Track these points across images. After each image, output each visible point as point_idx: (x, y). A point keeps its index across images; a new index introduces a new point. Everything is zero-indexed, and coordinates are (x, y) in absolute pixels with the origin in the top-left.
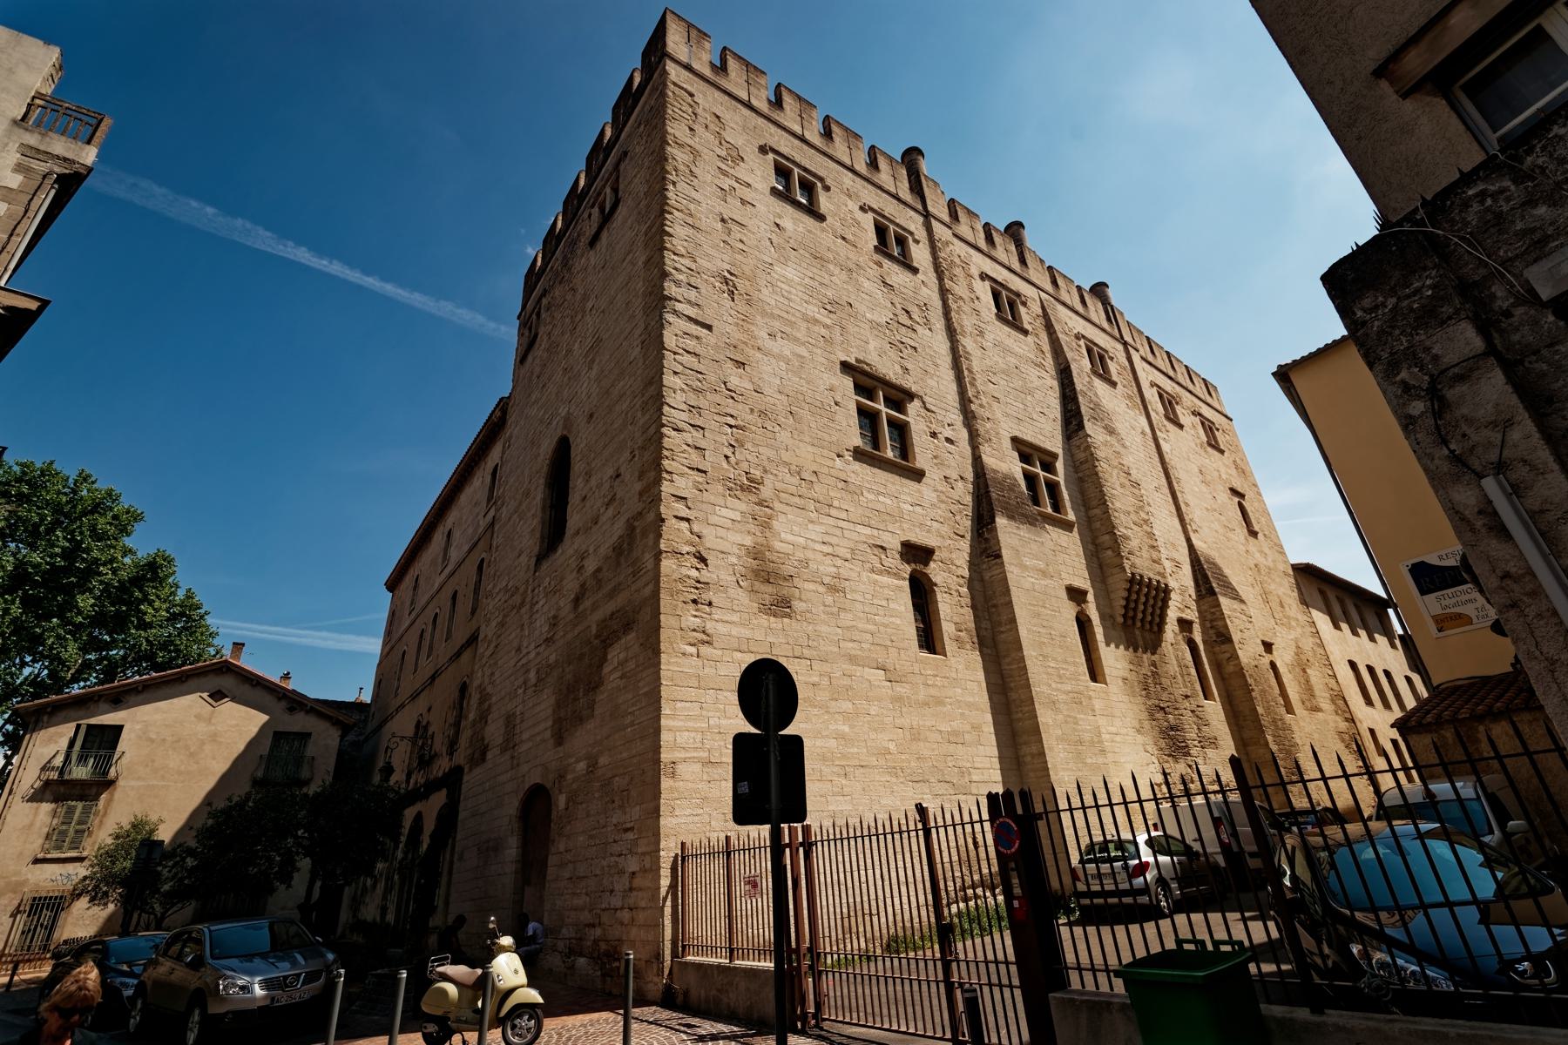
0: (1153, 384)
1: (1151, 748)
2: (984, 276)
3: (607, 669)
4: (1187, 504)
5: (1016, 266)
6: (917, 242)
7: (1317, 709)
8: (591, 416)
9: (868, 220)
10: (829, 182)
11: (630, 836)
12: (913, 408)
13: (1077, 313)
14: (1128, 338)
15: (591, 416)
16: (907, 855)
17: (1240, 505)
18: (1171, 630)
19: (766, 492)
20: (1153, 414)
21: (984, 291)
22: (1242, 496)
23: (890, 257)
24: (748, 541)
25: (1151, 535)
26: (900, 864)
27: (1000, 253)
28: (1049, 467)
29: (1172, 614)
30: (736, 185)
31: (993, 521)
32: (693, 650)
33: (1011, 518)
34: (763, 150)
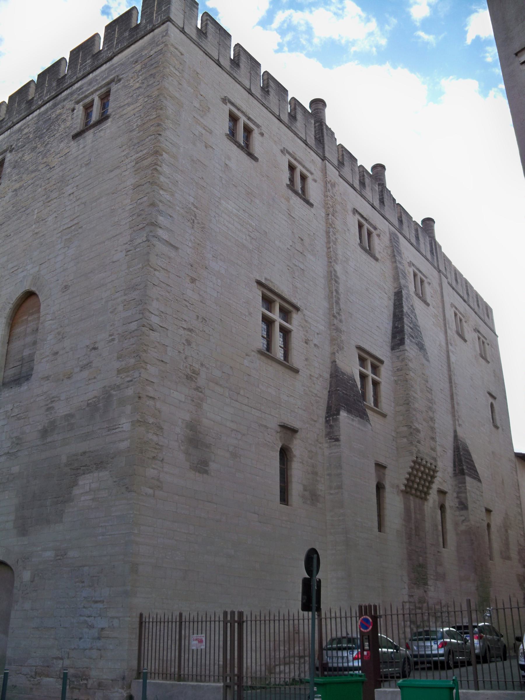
0: (452, 305)
1: (406, 579)
2: (355, 211)
3: (76, 491)
4: (458, 404)
5: (377, 204)
6: (315, 181)
7: (508, 558)
8: (66, 287)
9: (284, 161)
10: (264, 130)
11: (100, 605)
12: (296, 317)
13: (412, 244)
14: (442, 268)
15: (66, 287)
16: (258, 634)
17: (492, 405)
18: (433, 497)
19: (201, 381)
20: (449, 331)
21: (353, 221)
22: (494, 398)
23: (296, 192)
24: (187, 417)
25: (433, 429)
26: (254, 639)
27: (368, 193)
28: (375, 369)
29: (435, 487)
30: (204, 132)
31: (338, 414)
32: (150, 491)
33: (349, 412)
34: (225, 100)
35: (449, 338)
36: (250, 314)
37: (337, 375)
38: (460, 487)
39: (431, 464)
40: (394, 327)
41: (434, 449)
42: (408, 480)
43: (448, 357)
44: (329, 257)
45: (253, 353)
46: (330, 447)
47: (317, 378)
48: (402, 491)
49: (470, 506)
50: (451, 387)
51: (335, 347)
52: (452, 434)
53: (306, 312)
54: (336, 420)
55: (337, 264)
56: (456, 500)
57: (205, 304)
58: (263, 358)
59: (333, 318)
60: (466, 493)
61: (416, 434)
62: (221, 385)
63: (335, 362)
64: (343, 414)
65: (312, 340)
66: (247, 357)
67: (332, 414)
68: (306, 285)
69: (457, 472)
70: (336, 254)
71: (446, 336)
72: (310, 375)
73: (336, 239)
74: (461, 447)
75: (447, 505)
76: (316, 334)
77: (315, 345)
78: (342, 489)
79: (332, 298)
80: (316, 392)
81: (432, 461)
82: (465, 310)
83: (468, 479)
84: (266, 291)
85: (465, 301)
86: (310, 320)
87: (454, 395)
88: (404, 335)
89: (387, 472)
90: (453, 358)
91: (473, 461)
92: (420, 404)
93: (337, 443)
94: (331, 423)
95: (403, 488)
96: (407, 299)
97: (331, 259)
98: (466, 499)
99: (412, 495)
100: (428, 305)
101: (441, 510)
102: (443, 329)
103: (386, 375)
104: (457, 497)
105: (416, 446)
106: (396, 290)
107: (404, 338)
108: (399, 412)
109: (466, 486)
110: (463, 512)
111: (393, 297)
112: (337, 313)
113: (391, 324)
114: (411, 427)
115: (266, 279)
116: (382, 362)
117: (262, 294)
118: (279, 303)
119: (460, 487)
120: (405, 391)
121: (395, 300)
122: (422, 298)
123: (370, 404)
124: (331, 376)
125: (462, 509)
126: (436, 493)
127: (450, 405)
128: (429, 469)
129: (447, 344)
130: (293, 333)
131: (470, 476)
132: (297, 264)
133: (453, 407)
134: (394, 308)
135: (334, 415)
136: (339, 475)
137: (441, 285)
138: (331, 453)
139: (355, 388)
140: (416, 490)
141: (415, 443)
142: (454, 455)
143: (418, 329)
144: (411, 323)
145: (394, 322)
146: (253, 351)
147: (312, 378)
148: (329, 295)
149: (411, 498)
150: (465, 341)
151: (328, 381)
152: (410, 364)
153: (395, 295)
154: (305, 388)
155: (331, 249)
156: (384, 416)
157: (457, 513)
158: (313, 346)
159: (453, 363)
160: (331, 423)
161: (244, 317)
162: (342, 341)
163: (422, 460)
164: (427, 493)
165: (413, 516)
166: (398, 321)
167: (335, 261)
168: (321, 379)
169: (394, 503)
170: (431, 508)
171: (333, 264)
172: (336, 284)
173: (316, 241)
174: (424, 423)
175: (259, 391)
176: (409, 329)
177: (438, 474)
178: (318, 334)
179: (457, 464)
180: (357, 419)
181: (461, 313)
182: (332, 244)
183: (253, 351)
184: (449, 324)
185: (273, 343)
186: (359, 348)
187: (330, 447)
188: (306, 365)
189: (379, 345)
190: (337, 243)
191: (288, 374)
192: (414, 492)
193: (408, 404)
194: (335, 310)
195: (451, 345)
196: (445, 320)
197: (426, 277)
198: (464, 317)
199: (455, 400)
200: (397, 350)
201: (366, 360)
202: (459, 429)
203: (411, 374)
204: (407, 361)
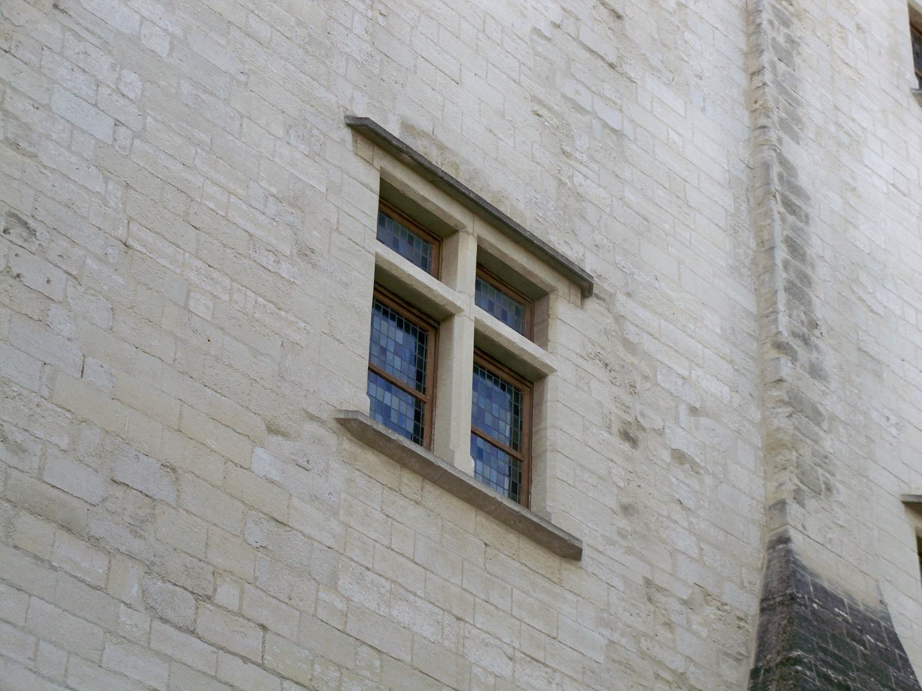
36: (305, 253)
37: (793, 598)
44: (756, 106)
45: (311, 428)
47: (684, 602)
51: (784, 476)
53: (624, 305)
55: (796, 138)
57: (33, 156)
58: (370, 458)
59: (774, 353)
62: (94, 542)
65: (660, 433)
66: (275, 439)
68: (630, 196)
70: (793, 102)
72: (648, 583)
73: (791, 40)
76: (683, 411)
77: (679, 457)
79: (770, 269)
80: (678, 664)
84: (403, 177)
86: (648, 345)
97: (768, 110)
112: (794, 335)
115: (407, 126)
117: (383, 182)
118: (480, 240)
124: (767, 606)
130: (551, 382)
132: (585, 100)
139: (892, 671)
146: (313, 418)
147: (657, 596)
148: (754, 262)
151: (752, 629)
154: (616, 637)
155: (768, 77)
158: (666, 456)
161: (269, 260)
162: (824, 459)
167: (785, 126)
168: (710, 611)
171: (773, 135)
172: (791, 218)
173: (688, 36)
175: (340, 605)
178: (694, 411)
182: (768, 57)
183: (313, 418)
185: (439, 411)
188: (622, 534)
190: (797, 60)
191: (520, 558)
194: (783, 319)
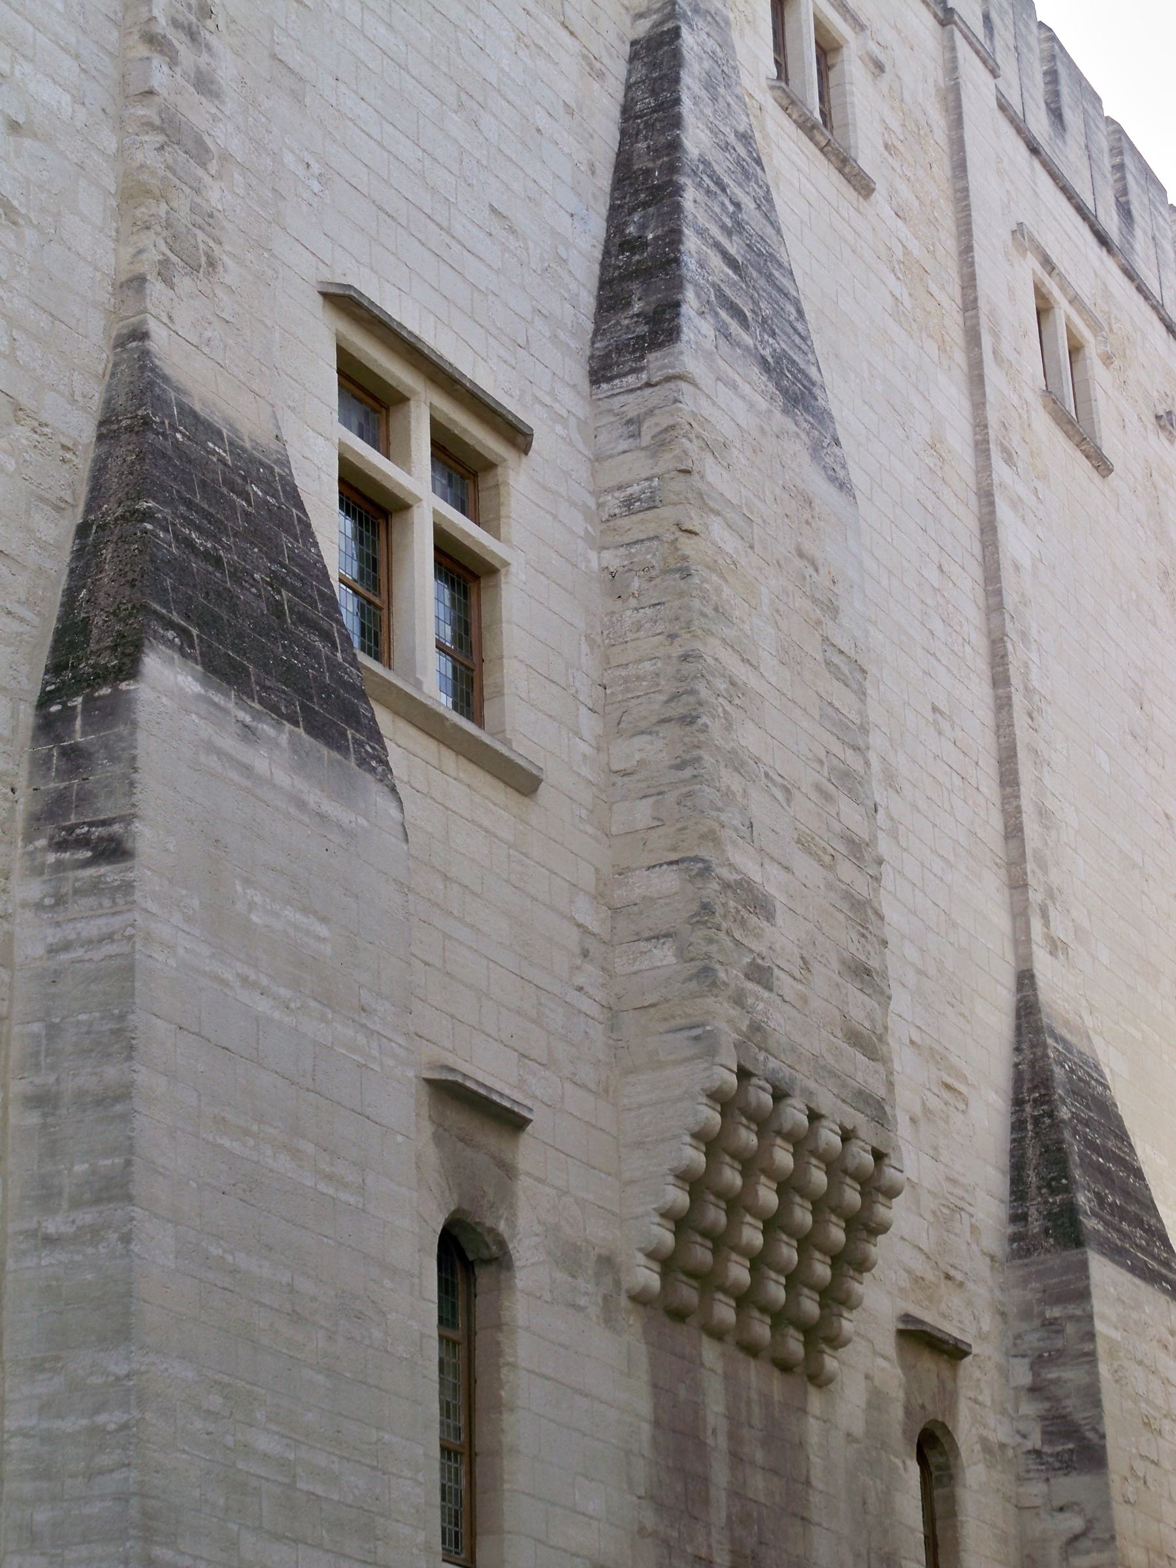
4: (1043, 814)
18: (867, 1366)
25: (863, 912)
31: (129, 669)
33: (222, 670)
35: (993, 417)
37: (146, 422)
38: (1051, 1326)
39: (847, 1136)
40: (618, 243)
41: (868, 1043)
42: (681, 1223)
43: (988, 528)
46: (60, 901)
48: (640, 1299)
49: (1120, 1446)
50: (1003, 705)
51: (146, 239)
52: (1005, 997)
54: (112, 712)
56: (1030, 1408)
59: (143, 50)
60: (1090, 1358)
61: (743, 923)
63: (144, 336)
64: (166, 682)
67: (84, 670)
69: (1035, 1226)
71: (979, 404)
74: (1059, 1073)
75: (968, 1432)
78: (129, 1198)
81: (858, 1120)
82: (1107, 293)
83: (1103, 1273)
85: (1103, 240)
87: (1022, 754)
88: (677, 284)
89: (527, 1153)
90: (1016, 542)
91: (1139, 1174)
92: (771, 730)
93: (109, 872)
94: (79, 735)
95: (648, 1277)
96: (710, 85)
98: (1092, 1395)
99: (717, 1334)
100: (862, 185)
101: (922, 1459)
102: (960, 357)
103: (538, 524)
104: (1035, 1390)
105: (738, 1000)
106: (643, 28)
107: (677, 305)
108: (626, 774)
109: (1090, 1317)
110: (1071, 1486)
111: (617, 69)
112: (175, 23)
113: (598, 227)
114: (706, 871)
116: (517, 436)
119: (1051, 1326)
120: (672, 637)
121: (629, 87)
122: (824, 127)
123: (418, 685)
124: (109, 430)
125: (1066, 1465)
126: (888, 1344)
127: (996, 821)
128: (835, 1167)
129: (982, 448)
131: (1116, 1254)
133: (1014, 831)
134: (623, 132)
135: (103, 676)
136: (115, 1100)
137: (953, 102)
138: (67, 946)
139: (285, 540)
140: (744, 1300)
141: (731, 975)
142: (1018, 1126)
143: (785, 282)
144: (729, 233)
145: (616, 215)
149: (710, 1353)
150: (1102, 465)
151: (84, 465)
152: (713, 473)
153: (633, 58)
156: (522, 781)
157: (1036, 1490)
159: (1017, 568)
160: (79, 735)
163: (779, 1095)
164: (821, 1336)
165: (720, 1475)
166: (645, 205)
169: (575, 1374)
170: (850, 1437)
174: (802, 863)
176: (716, 261)
177: (898, 1214)
179: (1032, 1178)
180: (284, 735)
181: (1074, 300)
184: (996, 335)
186: (345, 303)
187: (60, 901)
189: (507, 315)
192: (725, 1312)
193: (688, 720)
195: (1009, 459)
196: (970, 305)
197: (858, 25)
198: (1095, 326)
199: (1027, 790)
200: (631, 379)
201: (402, 399)
202: (1044, 967)
203: (717, 530)
204: (693, 447)
